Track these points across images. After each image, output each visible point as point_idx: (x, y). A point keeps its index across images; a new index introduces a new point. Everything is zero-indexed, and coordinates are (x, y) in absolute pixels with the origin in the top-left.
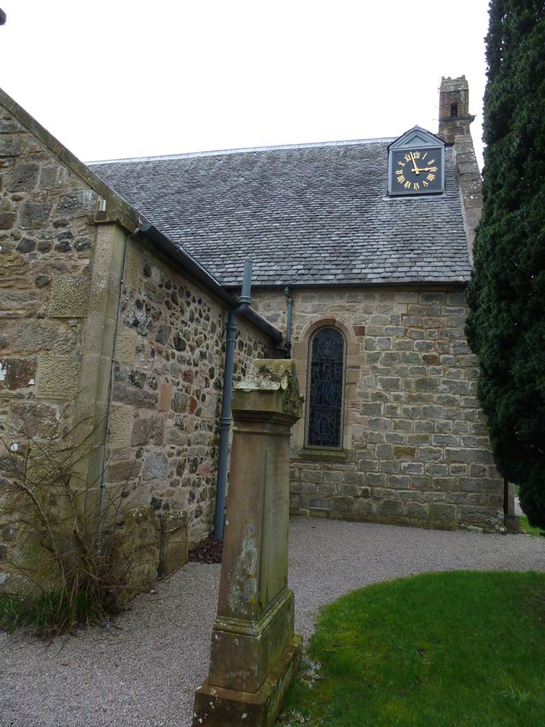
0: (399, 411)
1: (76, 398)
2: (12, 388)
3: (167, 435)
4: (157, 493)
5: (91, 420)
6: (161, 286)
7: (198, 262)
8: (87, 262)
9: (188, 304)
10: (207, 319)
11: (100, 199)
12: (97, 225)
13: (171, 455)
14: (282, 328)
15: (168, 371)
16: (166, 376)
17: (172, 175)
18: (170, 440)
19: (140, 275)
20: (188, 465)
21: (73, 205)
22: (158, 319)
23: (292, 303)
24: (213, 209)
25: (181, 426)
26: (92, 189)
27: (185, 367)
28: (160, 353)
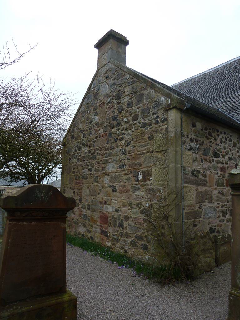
1: (168, 184)
2: (145, 182)
3: (214, 198)
4: (212, 225)
5: (174, 193)
6: (202, 130)
7: (229, 114)
8: (166, 126)
9: (218, 135)
10: (230, 140)
11: (167, 99)
12: (168, 110)
13: (218, 207)
15: (211, 168)
16: (210, 170)
17: (212, 78)
18: (217, 200)
19: (190, 127)
20: (228, 212)
21: (158, 104)
22: (203, 145)
24: (234, 87)
25: (222, 194)
26: (164, 96)
27: (220, 165)
28: (206, 160)
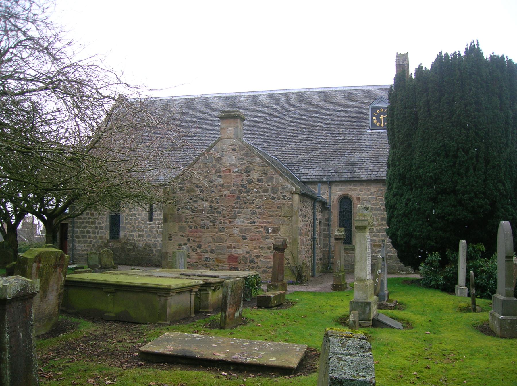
0: (374, 230)
14: (327, 198)
23: (331, 188)
